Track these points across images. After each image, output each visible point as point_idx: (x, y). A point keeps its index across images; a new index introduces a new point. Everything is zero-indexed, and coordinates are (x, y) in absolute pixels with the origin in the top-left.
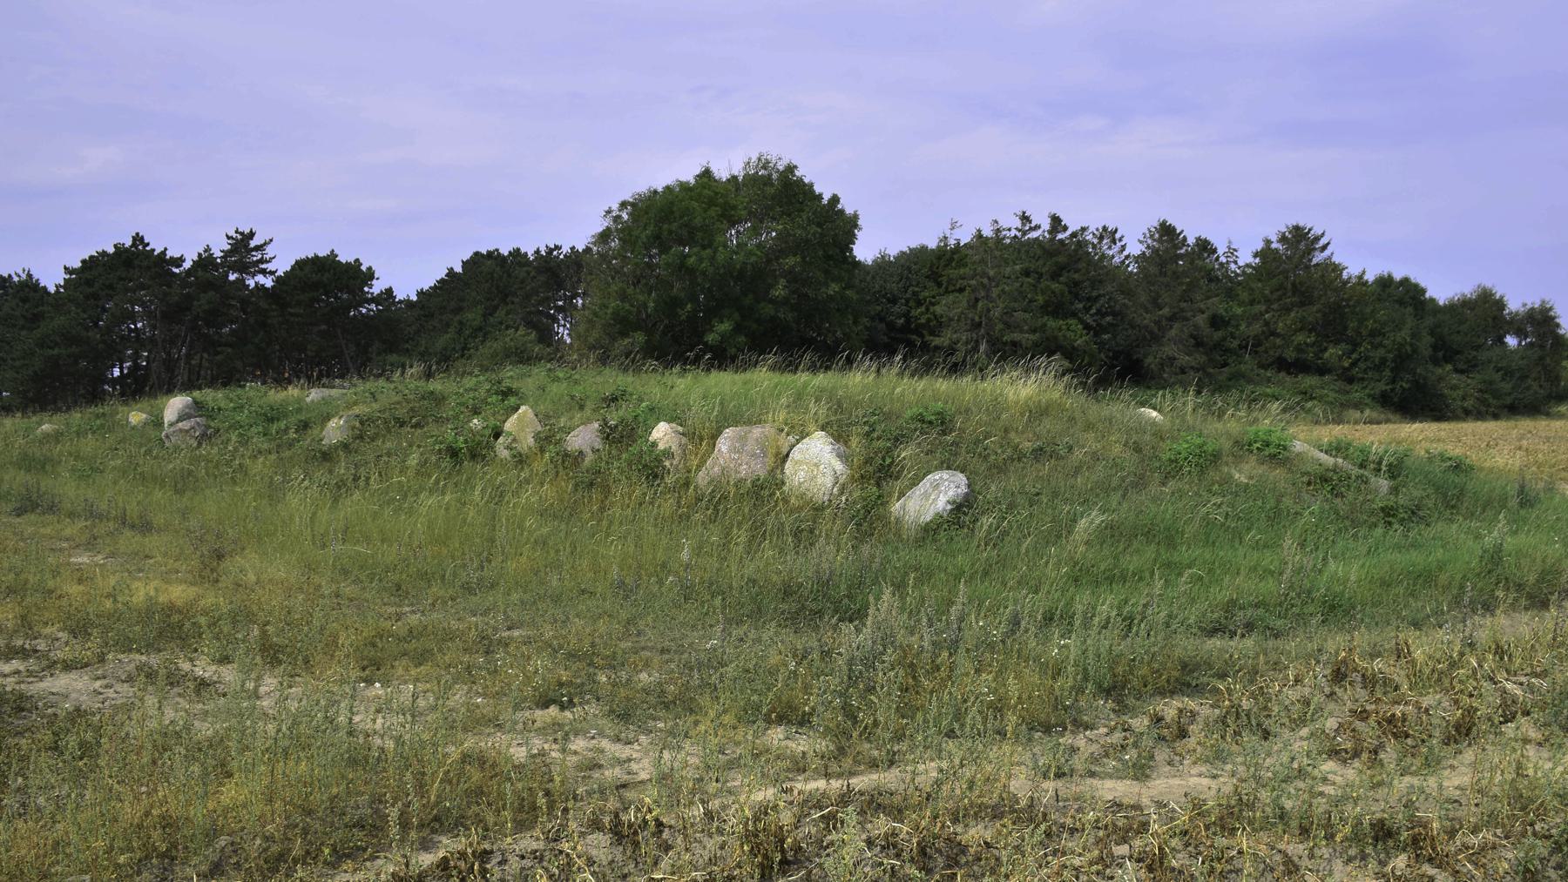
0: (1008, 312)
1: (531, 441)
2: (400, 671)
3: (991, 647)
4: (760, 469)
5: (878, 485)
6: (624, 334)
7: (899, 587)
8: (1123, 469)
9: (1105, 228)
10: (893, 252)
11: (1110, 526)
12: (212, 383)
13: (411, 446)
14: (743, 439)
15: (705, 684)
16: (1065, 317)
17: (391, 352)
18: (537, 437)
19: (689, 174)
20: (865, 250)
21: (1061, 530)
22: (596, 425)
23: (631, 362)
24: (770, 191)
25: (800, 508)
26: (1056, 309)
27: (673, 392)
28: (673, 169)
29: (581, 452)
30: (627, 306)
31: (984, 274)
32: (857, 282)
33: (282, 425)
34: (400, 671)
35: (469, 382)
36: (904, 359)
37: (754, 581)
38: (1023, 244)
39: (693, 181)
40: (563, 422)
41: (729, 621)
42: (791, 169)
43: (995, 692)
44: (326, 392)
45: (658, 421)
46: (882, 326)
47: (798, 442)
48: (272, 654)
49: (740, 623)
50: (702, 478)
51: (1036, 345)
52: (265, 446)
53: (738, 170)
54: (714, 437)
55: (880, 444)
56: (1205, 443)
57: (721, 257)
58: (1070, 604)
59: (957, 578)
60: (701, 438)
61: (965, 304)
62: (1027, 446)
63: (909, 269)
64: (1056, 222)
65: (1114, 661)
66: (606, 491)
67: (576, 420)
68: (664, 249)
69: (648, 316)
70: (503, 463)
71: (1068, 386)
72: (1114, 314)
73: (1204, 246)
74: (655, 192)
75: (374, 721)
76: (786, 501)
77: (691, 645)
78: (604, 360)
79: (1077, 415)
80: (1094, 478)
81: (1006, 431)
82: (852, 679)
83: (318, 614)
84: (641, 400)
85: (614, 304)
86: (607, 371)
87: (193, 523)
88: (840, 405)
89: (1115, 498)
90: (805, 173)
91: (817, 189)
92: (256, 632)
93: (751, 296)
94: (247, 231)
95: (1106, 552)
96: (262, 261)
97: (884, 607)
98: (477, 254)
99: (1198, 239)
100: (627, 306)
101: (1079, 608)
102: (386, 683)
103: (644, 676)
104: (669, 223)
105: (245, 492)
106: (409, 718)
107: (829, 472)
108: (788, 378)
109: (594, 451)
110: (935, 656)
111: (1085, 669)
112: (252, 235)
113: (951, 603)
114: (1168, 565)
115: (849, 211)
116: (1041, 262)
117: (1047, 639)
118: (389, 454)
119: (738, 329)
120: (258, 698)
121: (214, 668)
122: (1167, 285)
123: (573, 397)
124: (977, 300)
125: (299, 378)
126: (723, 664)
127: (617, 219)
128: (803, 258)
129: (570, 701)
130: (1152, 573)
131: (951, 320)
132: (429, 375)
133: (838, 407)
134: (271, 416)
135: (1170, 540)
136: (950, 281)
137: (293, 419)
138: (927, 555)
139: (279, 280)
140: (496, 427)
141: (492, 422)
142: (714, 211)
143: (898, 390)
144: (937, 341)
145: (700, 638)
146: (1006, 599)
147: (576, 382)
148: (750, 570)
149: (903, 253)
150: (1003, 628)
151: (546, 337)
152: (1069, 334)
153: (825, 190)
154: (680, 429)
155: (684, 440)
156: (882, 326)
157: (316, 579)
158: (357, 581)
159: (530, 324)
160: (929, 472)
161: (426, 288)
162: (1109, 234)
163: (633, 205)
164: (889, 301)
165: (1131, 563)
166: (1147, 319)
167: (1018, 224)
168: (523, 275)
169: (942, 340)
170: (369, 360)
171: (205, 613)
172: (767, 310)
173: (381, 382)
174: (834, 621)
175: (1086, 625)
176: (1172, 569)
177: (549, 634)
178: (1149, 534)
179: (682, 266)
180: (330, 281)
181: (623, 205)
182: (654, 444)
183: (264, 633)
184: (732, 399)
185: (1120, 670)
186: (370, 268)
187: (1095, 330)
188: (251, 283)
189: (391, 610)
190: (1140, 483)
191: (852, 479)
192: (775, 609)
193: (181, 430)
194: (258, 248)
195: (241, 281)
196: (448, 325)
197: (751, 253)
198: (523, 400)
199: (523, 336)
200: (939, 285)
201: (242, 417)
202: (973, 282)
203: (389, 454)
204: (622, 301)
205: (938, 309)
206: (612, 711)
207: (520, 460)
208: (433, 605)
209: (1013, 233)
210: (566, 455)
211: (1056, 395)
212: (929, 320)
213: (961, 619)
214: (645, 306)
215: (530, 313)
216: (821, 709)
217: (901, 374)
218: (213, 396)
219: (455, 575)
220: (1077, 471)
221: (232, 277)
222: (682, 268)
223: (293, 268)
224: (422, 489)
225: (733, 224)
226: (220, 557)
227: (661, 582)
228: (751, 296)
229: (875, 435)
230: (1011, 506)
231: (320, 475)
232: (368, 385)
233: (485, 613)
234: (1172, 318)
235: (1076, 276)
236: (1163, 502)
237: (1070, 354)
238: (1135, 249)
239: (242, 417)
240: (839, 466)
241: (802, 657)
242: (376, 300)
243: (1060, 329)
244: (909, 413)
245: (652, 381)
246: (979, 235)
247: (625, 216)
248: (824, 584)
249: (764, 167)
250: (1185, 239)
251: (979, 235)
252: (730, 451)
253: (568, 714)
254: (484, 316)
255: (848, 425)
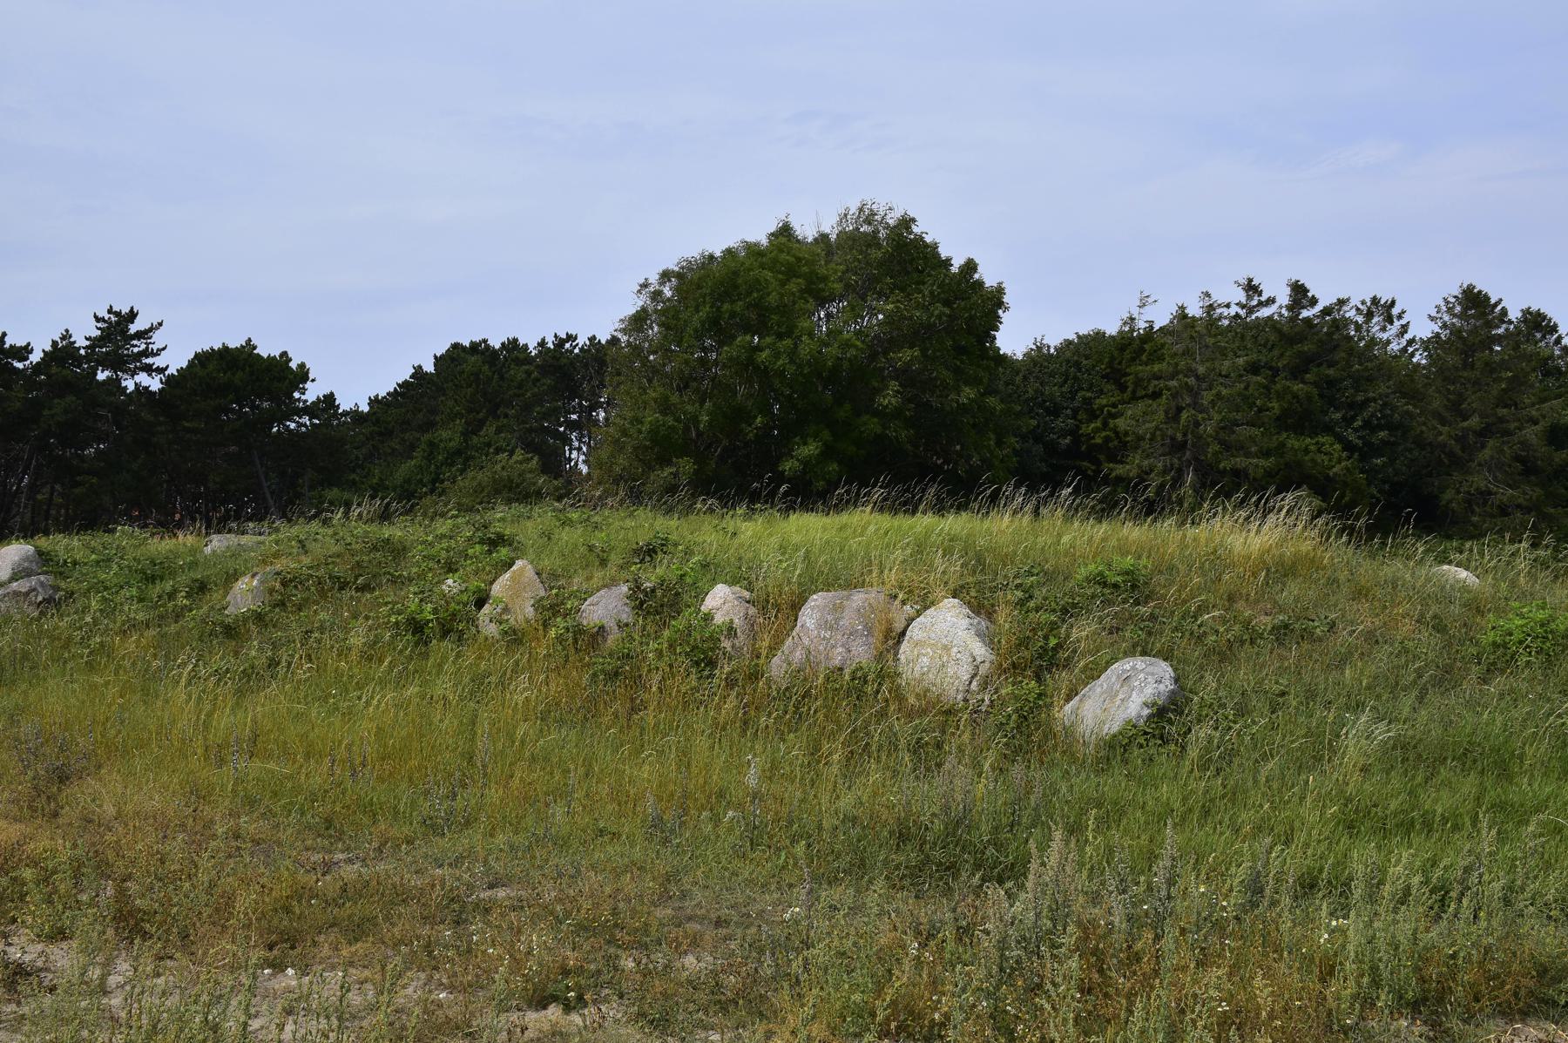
0: (1228, 426)
1: (530, 611)
2: (326, 950)
3: (1219, 927)
4: (862, 653)
5: (1039, 678)
6: (664, 461)
7: (1075, 830)
8: (1416, 657)
9: (1375, 301)
10: (1054, 341)
11: (1401, 745)
12: (66, 528)
13: (355, 617)
14: (838, 609)
15: (781, 975)
16: (1313, 434)
17: (331, 485)
18: (538, 605)
19: (759, 234)
20: (1012, 340)
21: (1320, 750)
22: (625, 589)
23: (670, 498)
24: (876, 254)
25: (923, 712)
26: (1300, 420)
27: (736, 541)
28: (731, 224)
29: (602, 628)
30: (670, 421)
31: (1191, 372)
32: (1001, 387)
33: (168, 586)
34: (326, 950)
35: (443, 526)
36: (1076, 492)
37: (854, 820)
38: (1247, 326)
39: (764, 241)
40: (577, 582)
41: (816, 879)
42: (906, 222)
43: (1230, 998)
44: (232, 540)
45: (714, 582)
46: (1039, 449)
47: (919, 613)
48: (130, 925)
49: (833, 881)
50: (777, 667)
51: (1270, 475)
52: (141, 616)
53: (830, 226)
54: (796, 606)
55: (1044, 617)
56: (1552, 619)
57: (806, 348)
58: (1343, 862)
59: (1161, 819)
60: (776, 609)
61: (1161, 415)
62: (1265, 622)
63: (1077, 365)
64: (1300, 293)
65: (1423, 958)
66: (637, 681)
67: (595, 582)
68: (724, 337)
69: (699, 434)
70: (489, 643)
71: (1325, 536)
72: (1392, 427)
73: (1537, 323)
74: (711, 257)
75: (281, 1027)
76: (901, 699)
77: (761, 913)
78: (636, 498)
79: (1343, 576)
80: (1372, 669)
81: (1231, 599)
82: (1007, 972)
83: (205, 862)
84: (688, 553)
85: (651, 417)
86: (640, 512)
87: (26, 728)
88: (980, 560)
89: (1407, 702)
90: (929, 228)
91: (944, 253)
92: (110, 891)
93: (847, 406)
94: (125, 310)
95: (1396, 781)
96: (146, 353)
97: (1053, 861)
98: (456, 346)
99: (1526, 312)
100: (670, 421)
101: (1358, 868)
102: (304, 971)
103: (690, 960)
104: (727, 299)
105: (107, 683)
106: (335, 1022)
107: (966, 659)
108: (903, 522)
109: (621, 626)
110: (1132, 939)
111: (1374, 969)
112: (132, 316)
113: (1152, 857)
114: (1499, 807)
115: (990, 282)
116: (1276, 352)
117: (1308, 920)
118: (322, 629)
119: (828, 453)
120: (105, 993)
121: (40, 947)
122: (1476, 383)
123: (591, 548)
124: (1180, 409)
125: (194, 520)
126: (807, 945)
127: (656, 296)
128: (924, 351)
129: (580, 998)
130: (1475, 821)
131: (1140, 438)
132: (385, 516)
133: (978, 561)
134: (151, 574)
135: (1504, 766)
136: (1138, 382)
137: (183, 579)
138: (1114, 784)
139: (170, 381)
140: (479, 590)
141: (475, 583)
142: (793, 286)
143: (1065, 539)
144: (1120, 470)
145: (775, 905)
146: (1239, 853)
147: (596, 527)
148: (846, 802)
149: (1068, 343)
150: (1236, 899)
151: (553, 464)
152: (1320, 458)
153: (955, 252)
154: (747, 594)
155: (752, 611)
156: (1039, 449)
157: (207, 811)
158: (268, 814)
159: (529, 447)
160: (1115, 660)
161: (382, 394)
162: (1383, 309)
163: (679, 276)
164: (1048, 412)
165: (1439, 802)
166: (1445, 434)
167: (1241, 296)
168: (521, 376)
169: (1128, 468)
170: (299, 496)
171: (34, 863)
172: (872, 425)
173: (315, 525)
174: (976, 880)
175: (1372, 898)
176: (1510, 814)
177: (550, 895)
178: (1466, 757)
179: (751, 361)
180: (244, 382)
181: (666, 276)
182: (708, 618)
183: (121, 893)
184: (821, 551)
185: (1433, 972)
186: (302, 366)
187: (1363, 452)
188: (129, 384)
189: (316, 857)
190: (1446, 678)
191: (1000, 670)
192: (886, 862)
193: (16, 594)
194: (141, 335)
195: (114, 383)
196: (413, 447)
197: (847, 345)
198: (519, 551)
199: (519, 463)
200: (1122, 388)
201: (108, 575)
202: (1174, 383)
203: (322, 629)
204: (664, 413)
205: (1121, 424)
206: (642, 1015)
207: (514, 638)
208: (379, 850)
209: (1234, 310)
210: (579, 631)
211: (1306, 547)
212: (1107, 439)
213: (1171, 882)
214: (695, 420)
215: (531, 430)
216: (958, 1016)
217: (1068, 519)
218: (64, 545)
219: (413, 804)
220: (1342, 661)
221: (102, 376)
222: (748, 366)
223: (191, 363)
224: (368, 679)
225: (822, 302)
226: (63, 778)
227: (716, 820)
228: (847, 406)
229: (1032, 604)
230: (1242, 711)
231: (219, 659)
232: (295, 530)
233: (456, 863)
234: (1484, 433)
235: (1331, 372)
236: (1485, 710)
237: (1321, 486)
238: (1423, 329)
239: (108, 575)
240: (980, 650)
241: (927, 936)
242: (311, 410)
243: (1307, 451)
244: (1082, 573)
245: (706, 527)
246: (1182, 315)
247: (668, 292)
248: (957, 824)
249: (868, 221)
250: (1504, 312)
251: (1182, 315)
252: (819, 627)
253: (576, 1018)
254: (465, 434)
255: (993, 590)
